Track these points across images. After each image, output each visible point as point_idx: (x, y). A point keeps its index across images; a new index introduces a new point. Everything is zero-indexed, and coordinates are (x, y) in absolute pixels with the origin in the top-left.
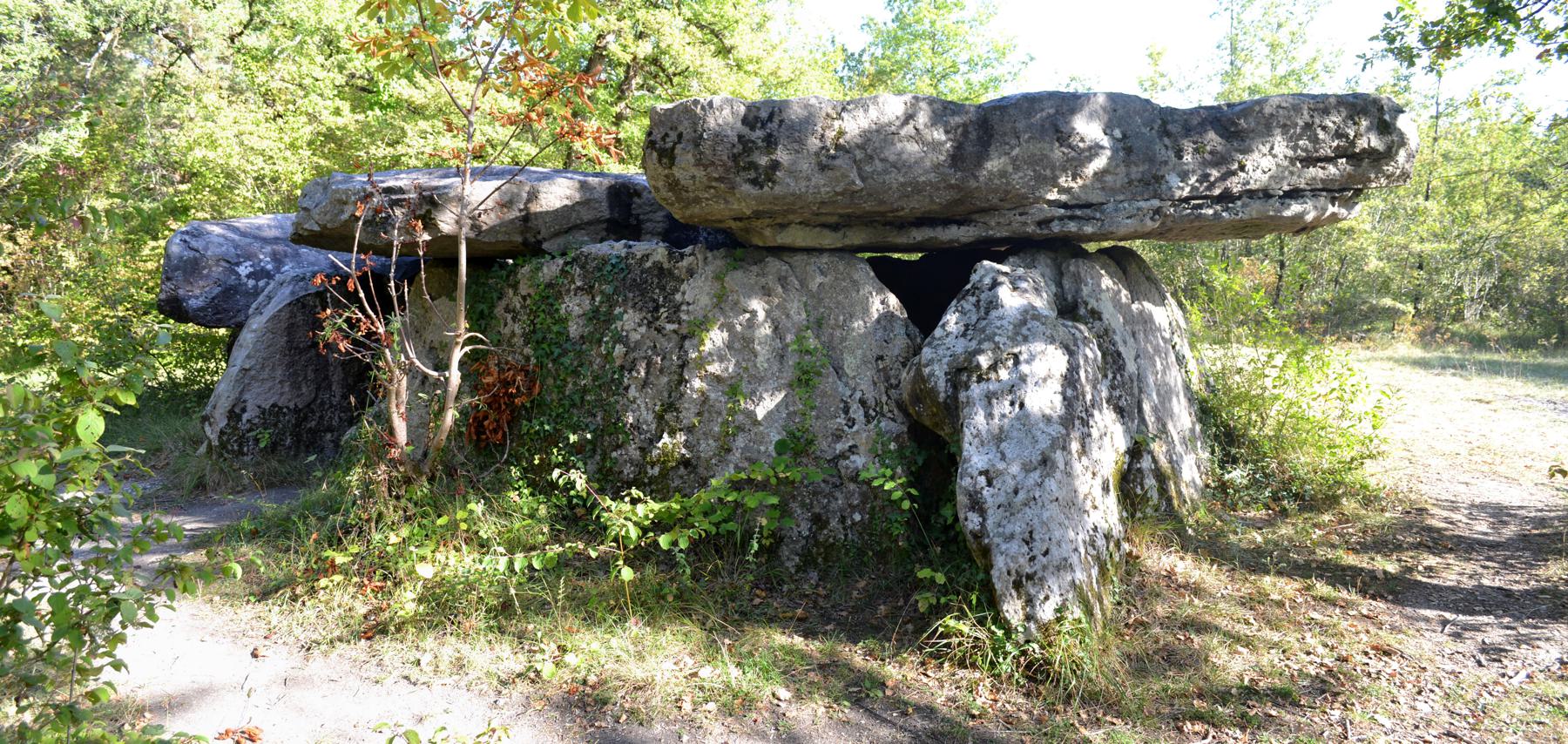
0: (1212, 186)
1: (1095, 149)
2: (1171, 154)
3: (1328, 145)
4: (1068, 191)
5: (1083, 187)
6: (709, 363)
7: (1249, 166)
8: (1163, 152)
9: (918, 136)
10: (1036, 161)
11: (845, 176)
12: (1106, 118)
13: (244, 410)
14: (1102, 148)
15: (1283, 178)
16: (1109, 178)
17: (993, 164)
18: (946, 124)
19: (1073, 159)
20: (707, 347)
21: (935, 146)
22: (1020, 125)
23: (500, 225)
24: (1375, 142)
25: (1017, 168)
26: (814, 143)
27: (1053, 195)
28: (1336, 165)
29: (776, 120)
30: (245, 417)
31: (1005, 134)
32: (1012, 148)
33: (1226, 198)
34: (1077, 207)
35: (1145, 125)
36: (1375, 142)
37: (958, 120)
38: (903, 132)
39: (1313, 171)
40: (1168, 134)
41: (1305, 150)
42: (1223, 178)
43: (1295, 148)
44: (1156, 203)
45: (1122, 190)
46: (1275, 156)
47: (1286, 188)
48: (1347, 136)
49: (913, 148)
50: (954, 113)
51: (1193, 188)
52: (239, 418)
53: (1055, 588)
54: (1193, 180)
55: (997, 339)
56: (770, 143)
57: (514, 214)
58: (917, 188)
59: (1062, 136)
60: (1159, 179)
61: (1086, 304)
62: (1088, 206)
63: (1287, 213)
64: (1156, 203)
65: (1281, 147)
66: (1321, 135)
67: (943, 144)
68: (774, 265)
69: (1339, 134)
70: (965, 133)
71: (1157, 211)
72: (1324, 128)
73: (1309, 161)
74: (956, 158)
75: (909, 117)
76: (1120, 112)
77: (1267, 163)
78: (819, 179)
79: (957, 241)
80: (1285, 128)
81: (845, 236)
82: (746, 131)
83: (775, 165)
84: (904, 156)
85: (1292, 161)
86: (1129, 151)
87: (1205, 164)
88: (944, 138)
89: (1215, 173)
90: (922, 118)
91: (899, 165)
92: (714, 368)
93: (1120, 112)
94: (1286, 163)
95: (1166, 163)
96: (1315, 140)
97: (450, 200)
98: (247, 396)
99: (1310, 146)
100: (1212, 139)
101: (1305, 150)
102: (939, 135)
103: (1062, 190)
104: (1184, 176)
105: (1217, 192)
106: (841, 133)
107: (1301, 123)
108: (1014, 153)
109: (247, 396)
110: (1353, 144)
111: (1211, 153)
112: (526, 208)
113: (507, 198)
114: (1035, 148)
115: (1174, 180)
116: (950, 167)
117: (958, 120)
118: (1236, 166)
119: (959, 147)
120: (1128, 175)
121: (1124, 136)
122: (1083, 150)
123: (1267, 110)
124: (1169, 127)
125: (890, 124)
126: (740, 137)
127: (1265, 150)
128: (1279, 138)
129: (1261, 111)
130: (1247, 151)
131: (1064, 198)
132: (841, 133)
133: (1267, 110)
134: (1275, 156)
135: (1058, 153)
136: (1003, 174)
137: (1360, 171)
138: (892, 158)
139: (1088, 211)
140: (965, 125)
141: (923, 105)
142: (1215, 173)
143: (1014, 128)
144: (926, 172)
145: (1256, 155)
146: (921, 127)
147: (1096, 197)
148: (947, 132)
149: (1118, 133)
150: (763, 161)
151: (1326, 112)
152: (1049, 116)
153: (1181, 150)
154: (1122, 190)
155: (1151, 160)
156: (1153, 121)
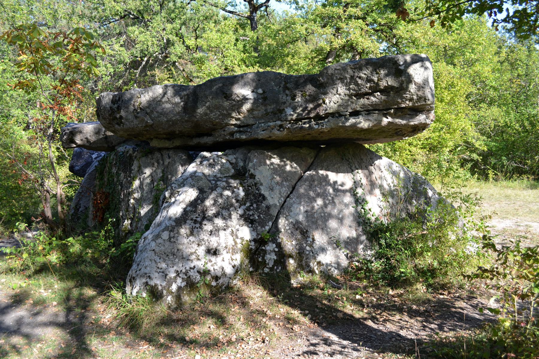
0: (310, 112)
1: (245, 99)
2: (289, 98)
3: (366, 87)
4: (237, 119)
5: (244, 117)
6: (134, 193)
7: (327, 101)
8: (283, 97)
9: (169, 101)
10: (218, 107)
11: (144, 120)
12: (254, 84)
13: (80, 207)
14: (247, 99)
15: (348, 105)
16: (256, 112)
17: (200, 110)
18: (180, 95)
19: (234, 105)
20: (134, 187)
21: (177, 104)
22: (207, 93)
23: (97, 140)
24: (390, 81)
25: (211, 111)
26: (132, 108)
27: (233, 122)
28: (374, 96)
29: (121, 100)
30: (80, 209)
31: (202, 97)
32: (206, 103)
33: (318, 118)
34: (243, 127)
35: (276, 86)
36: (390, 81)
37: (185, 93)
38: (163, 100)
39: (362, 101)
40: (288, 89)
41: (354, 90)
42: (315, 108)
43: (349, 89)
44: (279, 123)
45: (262, 117)
46: (340, 95)
47: (350, 111)
48: (373, 81)
49: (168, 106)
50: (184, 90)
51: (299, 114)
52: (78, 210)
53: (138, 284)
54: (299, 110)
55: (173, 185)
56: (119, 109)
57: (101, 136)
58: (175, 123)
59: (228, 96)
60: (281, 111)
61: (249, 171)
62: (247, 126)
63: (348, 124)
64: (279, 123)
65: (342, 89)
66: (360, 82)
67: (179, 103)
68: (157, 155)
69: (369, 80)
70: (188, 98)
71: (281, 126)
72: (360, 78)
73: (359, 96)
74: (185, 108)
75: (165, 93)
76: (263, 80)
77: (336, 98)
78: (136, 122)
79: (207, 143)
80: (342, 80)
81: (173, 143)
82: (112, 105)
83: (121, 117)
84: (165, 110)
85: (350, 96)
86: (265, 99)
87: (307, 101)
88: (180, 101)
89: (311, 106)
90: (170, 92)
91: (164, 113)
92: (136, 195)
93: (263, 80)
94: (347, 98)
95: (285, 103)
96: (357, 84)
97: (77, 132)
98: (81, 202)
99: (356, 88)
100: (310, 89)
101: (354, 90)
102: (177, 100)
103: (237, 119)
104: (294, 109)
105: (312, 115)
106: (141, 103)
107: (348, 76)
108: (207, 105)
109: (81, 202)
110: (377, 84)
111: (309, 96)
112: (105, 134)
113: (97, 131)
114: (216, 102)
115: (289, 111)
116: (184, 113)
117: (185, 93)
118: (321, 101)
119: (186, 104)
120: (266, 110)
121: (264, 92)
122: (238, 101)
123: (330, 72)
124: (288, 85)
125: (157, 97)
126: (111, 107)
127: (334, 91)
128: (340, 85)
129: (327, 73)
130: (325, 93)
131: (238, 122)
132: (141, 103)
133: (330, 72)
134: (340, 95)
135: (226, 104)
136: (206, 114)
137: (390, 98)
138: (160, 111)
139: (245, 128)
140: (187, 95)
141: (170, 88)
142: (311, 106)
143: (205, 94)
144: (175, 115)
145: (330, 95)
146: (169, 97)
147: (251, 122)
148: (181, 98)
149: (260, 91)
150: (118, 116)
151: (360, 69)
152: (220, 87)
153: (295, 96)
154: (262, 117)
155: (277, 102)
156: (281, 83)
